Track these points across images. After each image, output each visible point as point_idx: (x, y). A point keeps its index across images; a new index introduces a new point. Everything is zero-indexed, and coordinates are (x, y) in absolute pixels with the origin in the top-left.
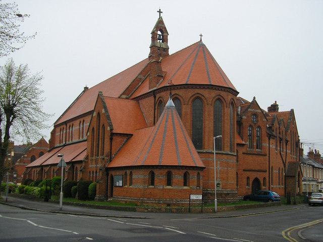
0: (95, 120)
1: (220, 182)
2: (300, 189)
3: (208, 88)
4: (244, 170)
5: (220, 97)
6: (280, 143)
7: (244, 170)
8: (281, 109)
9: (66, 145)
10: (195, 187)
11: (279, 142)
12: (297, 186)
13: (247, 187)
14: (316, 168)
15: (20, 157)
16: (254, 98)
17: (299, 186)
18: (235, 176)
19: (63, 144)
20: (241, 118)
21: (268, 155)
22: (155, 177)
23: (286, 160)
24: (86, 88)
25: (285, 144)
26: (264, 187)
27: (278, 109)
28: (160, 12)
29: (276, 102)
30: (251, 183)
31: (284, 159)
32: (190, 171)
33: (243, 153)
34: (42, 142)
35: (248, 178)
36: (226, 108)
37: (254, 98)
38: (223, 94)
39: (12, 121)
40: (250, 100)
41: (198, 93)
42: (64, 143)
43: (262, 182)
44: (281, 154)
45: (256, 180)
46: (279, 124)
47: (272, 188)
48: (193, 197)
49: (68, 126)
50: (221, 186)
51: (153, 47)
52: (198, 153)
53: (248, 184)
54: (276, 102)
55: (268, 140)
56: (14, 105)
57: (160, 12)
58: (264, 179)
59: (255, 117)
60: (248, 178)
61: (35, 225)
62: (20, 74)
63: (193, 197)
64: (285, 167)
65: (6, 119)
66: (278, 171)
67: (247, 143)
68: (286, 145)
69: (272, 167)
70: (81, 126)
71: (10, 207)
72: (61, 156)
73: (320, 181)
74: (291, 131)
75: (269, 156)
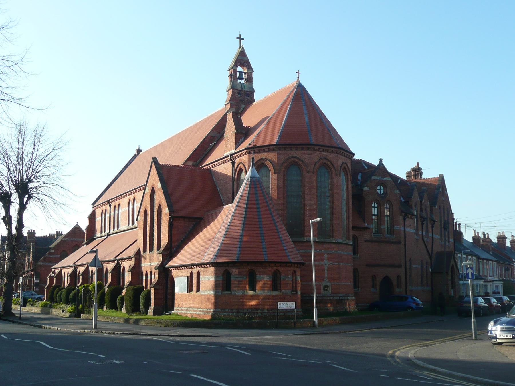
0: (148, 198)
1: (329, 284)
2: (455, 292)
3: (308, 149)
4: (367, 266)
5: (326, 161)
6: (422, 224)
7: (367, 266)
8: (426, 175)
9: (110, 235)
10: (289, 292)
11: (420, 223)
12: (450, 287)
13: (372, 290)
14: (483, 259)
15: (44, 254)
16: (381, 160)
17: (453, 287)
18: (352, 275)
19: (106, 234)
20: (362, 190)
21: (403, 243)
22: (232, 279)
23: (432, 250)
24: (139, 151)
25: (430, 226)
26: (397, 290)
27: (421, 173)
28: (240, 39)
29: (418, 163)
30: (378, 283)
31: (429, 247)
32: (281, 269)
33: (366, 241)
34: (76, 230)
35: (374, 277)
36: (334, 177)
37: (381, 160)
38: (330, 156)
39: (27, 203)
40: (376, 163)
41: (294, 157)
42: (107, 231)
43: (395, 283)
44: (423, 240)
45: (386, 280)
46: (421, 198)
47: (411, 291)
48: (282, 305)
49: (112, 207)
50: (330, 289)
51: (234, 88)
52: (294, 242)
53: (373, 286)
54: (418, 163)
55: (402, 222)
56: (30, 181)
57: (240, 39)
58: (399, 277)
59: (382, 188)
60: (374, 277)
61: (43, 343)
62: (37, 138)
63: (282, 305)
64: (431, 259)
65: (18, 201)
66: (419, 266)
67: (371, 226)
68: (432, 227)
69: (410, 260)
70: (131, 207)
71: (25, 326)
72: (94, 252)
73: (490, 278)
74: (440, 207)
75: (405, 245)
